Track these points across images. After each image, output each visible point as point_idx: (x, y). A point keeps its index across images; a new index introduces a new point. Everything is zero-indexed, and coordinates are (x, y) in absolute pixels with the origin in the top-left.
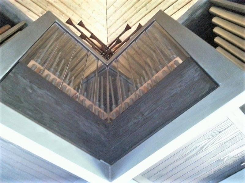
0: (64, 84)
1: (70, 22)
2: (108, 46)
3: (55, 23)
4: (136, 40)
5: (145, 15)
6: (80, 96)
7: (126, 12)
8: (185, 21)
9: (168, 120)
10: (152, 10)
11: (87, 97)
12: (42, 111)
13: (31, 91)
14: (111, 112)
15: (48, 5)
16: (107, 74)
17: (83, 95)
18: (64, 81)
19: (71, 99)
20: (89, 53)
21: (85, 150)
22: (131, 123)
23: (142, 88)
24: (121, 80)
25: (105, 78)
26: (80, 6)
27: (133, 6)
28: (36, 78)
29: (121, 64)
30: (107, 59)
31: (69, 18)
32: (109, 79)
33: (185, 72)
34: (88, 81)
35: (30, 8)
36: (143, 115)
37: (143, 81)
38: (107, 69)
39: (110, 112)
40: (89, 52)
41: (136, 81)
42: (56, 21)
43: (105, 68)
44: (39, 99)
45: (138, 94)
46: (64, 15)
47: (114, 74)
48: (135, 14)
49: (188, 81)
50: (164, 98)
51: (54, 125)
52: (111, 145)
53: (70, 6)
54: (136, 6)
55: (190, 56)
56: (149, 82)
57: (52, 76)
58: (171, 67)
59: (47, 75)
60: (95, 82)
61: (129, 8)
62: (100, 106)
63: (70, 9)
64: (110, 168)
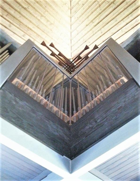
0: (39, 95)
1: (43, 44)
2: (71, 60)
3: (33, 48)
4: (92, 60)
5: (100, 37)
6: (49, 104)
7: (86, 34)
8: (131, 42)
9: (114, 129)
10: (106, 33)
11: (55, 105)
12: (22, 119)
13: (14, 103)
14: (72, 117)
15: (28, 30)
16: (69, 85)
17: (52, 103)
18: (39, 93)
19: (43, 107)
20: (57, 69)
21: (54, 149)
22: (87, 127)
23: (96, 99)
24: (80, 90)
25: (69, 87)
26: (51, 30)
27: (91, 30)
28: (19, 92)
29: (82, 74)
30: (70, 73)
31: (43, 41)
32: (71, 90)
33: (128, 90)
34: (56, 90)
35: (15, 32)
36: (96, 122)
37: (97, 93)
38: (70, 81)
39: (72, 116)
40: (57, 68)
41: (91, 93)
42: (34, 46)
43: (69, 80)
44: (20, 109)
45: (93, 103)
46: (39, 37)
47: (75, 84)
48: (93, 36)
49: (130, 98)
50: (113, 110)
51: (31, 129)
52: (72, 145)
53: (44, 30)
54: (93, 30)
55: (133, 78)
56: (102, 94)
57: (30, 90)
58: (118, 84)
59: (27, 89)
60: (61, 91)
61: (88, 31)
62: (64, 112)
63: (44, 32)
64: (70, 162)
